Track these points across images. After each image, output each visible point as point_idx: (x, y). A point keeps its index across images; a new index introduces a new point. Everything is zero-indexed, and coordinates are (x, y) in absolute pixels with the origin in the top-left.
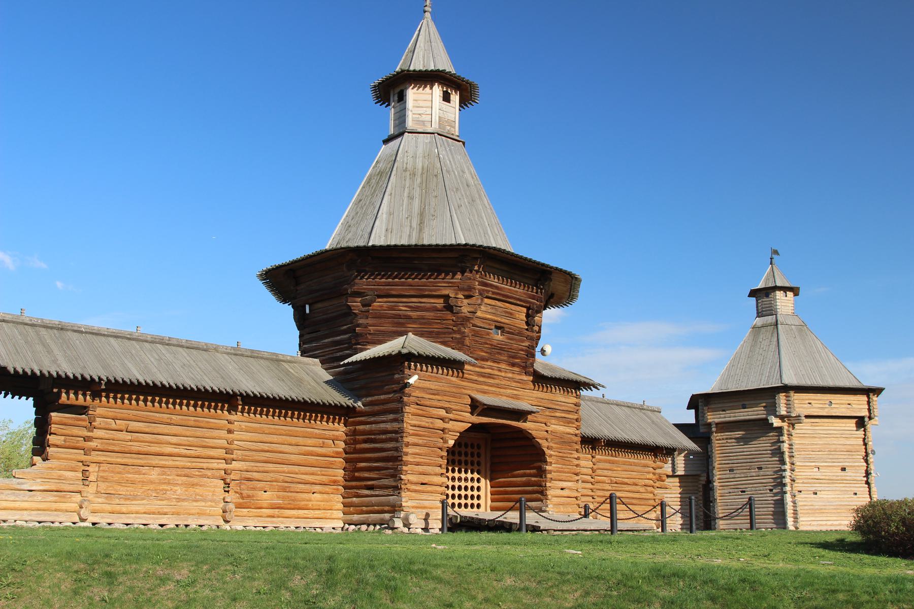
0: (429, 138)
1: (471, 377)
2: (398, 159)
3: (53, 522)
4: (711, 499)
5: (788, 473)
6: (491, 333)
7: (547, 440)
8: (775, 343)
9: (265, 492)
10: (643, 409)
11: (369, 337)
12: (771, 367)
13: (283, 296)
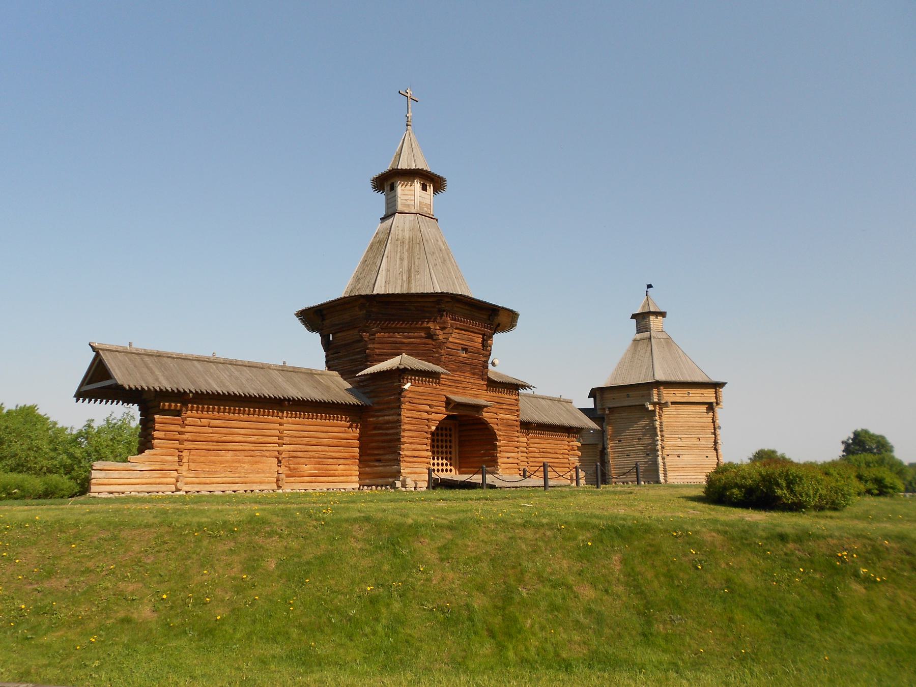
0: (413, 217)
1: (446, 383)
2: (392, 232)
3: (157, 492)
4: (606, 461)
5: (659, 442)
6: (459, 353)
7: (497, 424)
8: (649, 351)
9: (306, 465)
10: (561, 401)
11: (376, 356)
12: (647, 368)
13: (312, 327)
